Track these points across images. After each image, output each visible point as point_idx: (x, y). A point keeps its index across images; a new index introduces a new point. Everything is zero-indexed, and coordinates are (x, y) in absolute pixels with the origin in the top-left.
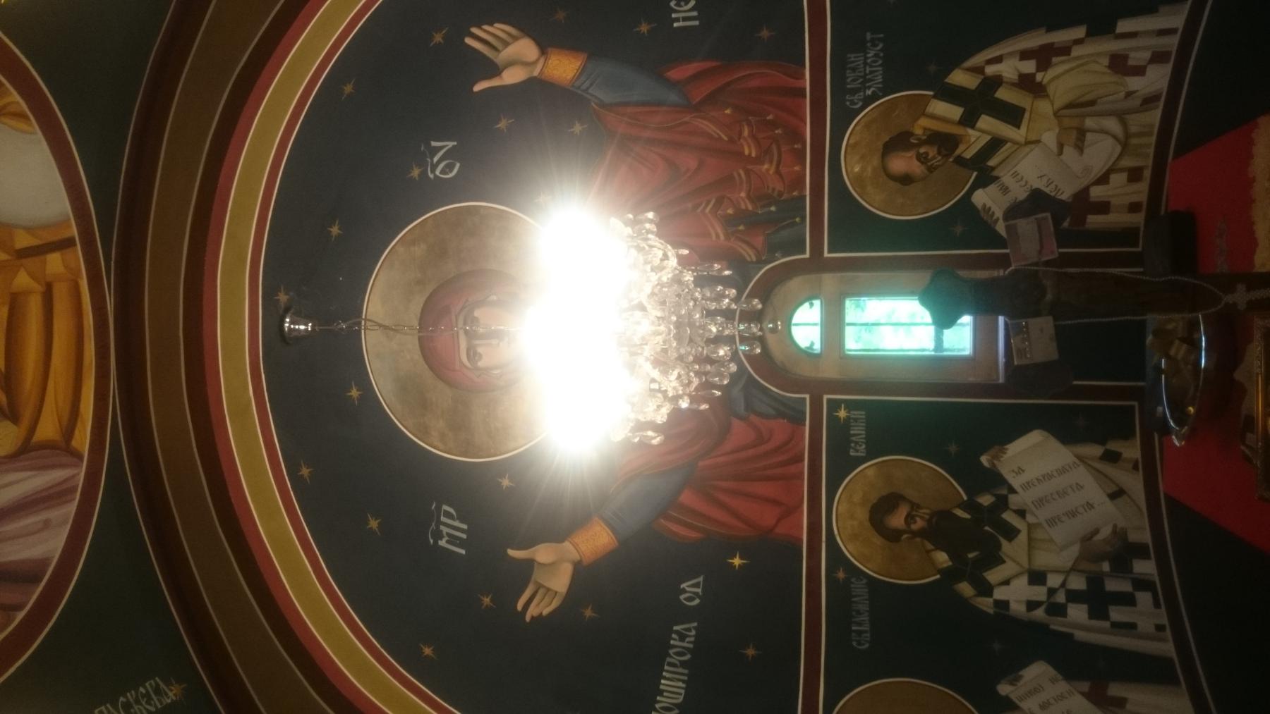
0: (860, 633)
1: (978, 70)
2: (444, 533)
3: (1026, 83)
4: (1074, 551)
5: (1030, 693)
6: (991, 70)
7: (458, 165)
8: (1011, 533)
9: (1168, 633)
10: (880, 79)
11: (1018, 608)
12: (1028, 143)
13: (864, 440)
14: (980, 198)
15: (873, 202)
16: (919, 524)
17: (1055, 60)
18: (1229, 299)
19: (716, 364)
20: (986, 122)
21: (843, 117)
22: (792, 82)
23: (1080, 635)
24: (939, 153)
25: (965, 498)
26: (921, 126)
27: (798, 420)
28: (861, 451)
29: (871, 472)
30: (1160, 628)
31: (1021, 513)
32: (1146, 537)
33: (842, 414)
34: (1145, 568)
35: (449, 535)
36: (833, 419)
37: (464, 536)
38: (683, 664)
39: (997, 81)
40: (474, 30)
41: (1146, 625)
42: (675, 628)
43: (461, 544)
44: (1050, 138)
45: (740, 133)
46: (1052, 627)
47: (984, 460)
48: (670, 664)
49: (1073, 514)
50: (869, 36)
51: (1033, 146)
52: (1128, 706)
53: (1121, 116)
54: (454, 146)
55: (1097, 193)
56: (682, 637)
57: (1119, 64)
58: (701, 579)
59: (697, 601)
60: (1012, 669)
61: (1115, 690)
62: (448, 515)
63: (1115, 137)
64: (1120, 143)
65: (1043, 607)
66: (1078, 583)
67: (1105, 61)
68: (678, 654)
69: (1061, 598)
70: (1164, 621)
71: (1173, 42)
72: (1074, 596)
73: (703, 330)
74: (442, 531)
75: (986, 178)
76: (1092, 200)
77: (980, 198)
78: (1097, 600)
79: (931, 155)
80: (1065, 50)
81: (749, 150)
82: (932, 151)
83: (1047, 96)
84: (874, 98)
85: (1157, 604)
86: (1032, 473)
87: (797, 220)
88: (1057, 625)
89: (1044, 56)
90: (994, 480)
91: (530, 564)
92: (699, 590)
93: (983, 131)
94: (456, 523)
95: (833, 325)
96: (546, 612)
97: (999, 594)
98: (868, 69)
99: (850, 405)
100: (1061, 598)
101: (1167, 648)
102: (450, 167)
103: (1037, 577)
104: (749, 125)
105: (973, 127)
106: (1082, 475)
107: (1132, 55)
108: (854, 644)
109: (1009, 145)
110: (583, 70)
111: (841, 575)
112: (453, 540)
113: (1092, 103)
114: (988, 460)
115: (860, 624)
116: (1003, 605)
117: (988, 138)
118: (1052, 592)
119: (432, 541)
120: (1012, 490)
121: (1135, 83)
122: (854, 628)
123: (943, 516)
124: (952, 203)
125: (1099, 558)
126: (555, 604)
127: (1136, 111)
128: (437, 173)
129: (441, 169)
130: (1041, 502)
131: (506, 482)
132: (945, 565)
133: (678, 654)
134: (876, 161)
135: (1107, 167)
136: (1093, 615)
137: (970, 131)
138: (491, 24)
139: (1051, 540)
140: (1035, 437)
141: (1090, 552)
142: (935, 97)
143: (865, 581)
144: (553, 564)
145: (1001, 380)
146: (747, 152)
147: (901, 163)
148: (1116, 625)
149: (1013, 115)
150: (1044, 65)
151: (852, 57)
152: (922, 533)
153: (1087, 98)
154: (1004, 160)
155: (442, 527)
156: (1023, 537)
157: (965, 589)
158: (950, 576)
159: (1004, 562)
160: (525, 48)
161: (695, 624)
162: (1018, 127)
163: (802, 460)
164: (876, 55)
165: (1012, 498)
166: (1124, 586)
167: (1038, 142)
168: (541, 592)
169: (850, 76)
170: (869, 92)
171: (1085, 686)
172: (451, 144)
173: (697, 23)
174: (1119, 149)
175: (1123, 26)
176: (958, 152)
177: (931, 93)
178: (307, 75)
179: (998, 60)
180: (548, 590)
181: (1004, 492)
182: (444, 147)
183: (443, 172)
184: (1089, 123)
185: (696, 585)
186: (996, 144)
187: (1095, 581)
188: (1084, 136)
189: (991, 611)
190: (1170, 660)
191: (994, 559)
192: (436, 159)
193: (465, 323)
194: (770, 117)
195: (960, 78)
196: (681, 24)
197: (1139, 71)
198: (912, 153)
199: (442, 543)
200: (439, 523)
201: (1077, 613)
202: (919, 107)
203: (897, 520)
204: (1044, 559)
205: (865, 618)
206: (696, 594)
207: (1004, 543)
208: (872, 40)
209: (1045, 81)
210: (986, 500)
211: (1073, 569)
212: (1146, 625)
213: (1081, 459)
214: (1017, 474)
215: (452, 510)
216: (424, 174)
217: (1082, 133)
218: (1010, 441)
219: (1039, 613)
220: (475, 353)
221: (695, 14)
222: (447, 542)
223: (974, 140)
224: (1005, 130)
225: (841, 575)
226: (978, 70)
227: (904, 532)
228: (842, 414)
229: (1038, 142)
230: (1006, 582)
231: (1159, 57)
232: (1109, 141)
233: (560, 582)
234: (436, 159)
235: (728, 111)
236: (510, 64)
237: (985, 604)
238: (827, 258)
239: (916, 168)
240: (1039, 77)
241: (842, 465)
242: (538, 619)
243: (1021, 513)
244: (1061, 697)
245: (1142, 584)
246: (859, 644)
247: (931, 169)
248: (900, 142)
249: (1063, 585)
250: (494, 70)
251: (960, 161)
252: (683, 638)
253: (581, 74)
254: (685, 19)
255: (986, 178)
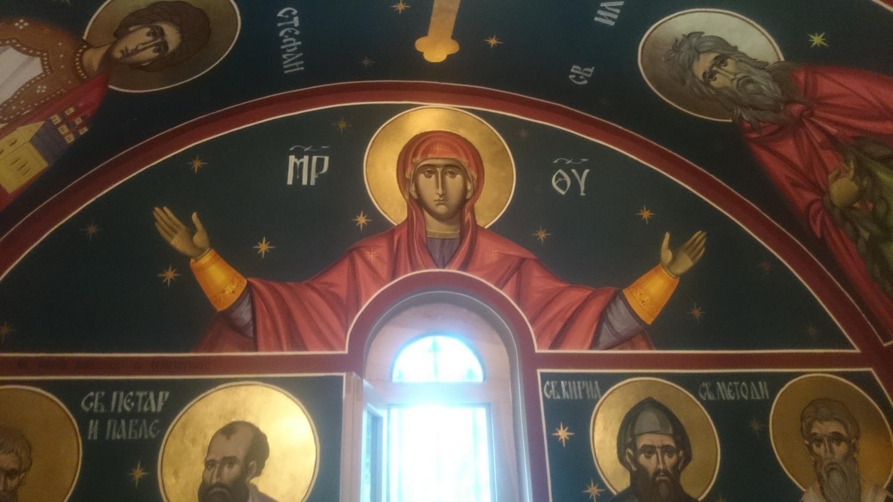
2: (301, 160)
7: (563, 193)
13: (739, 398)
19: (608, 311)
35: (302, 164)
62: (320, 163)
74: (303, 157)
102: (562, 185)
112: (298, 170)
119: (292, 149)
122: (562, 383)
161: (621, 3)
178: (567, 106)
199: (292, 159)
200: (311, 155)
215: (325, 169)
222: (295, 164)
234: (574, 171)
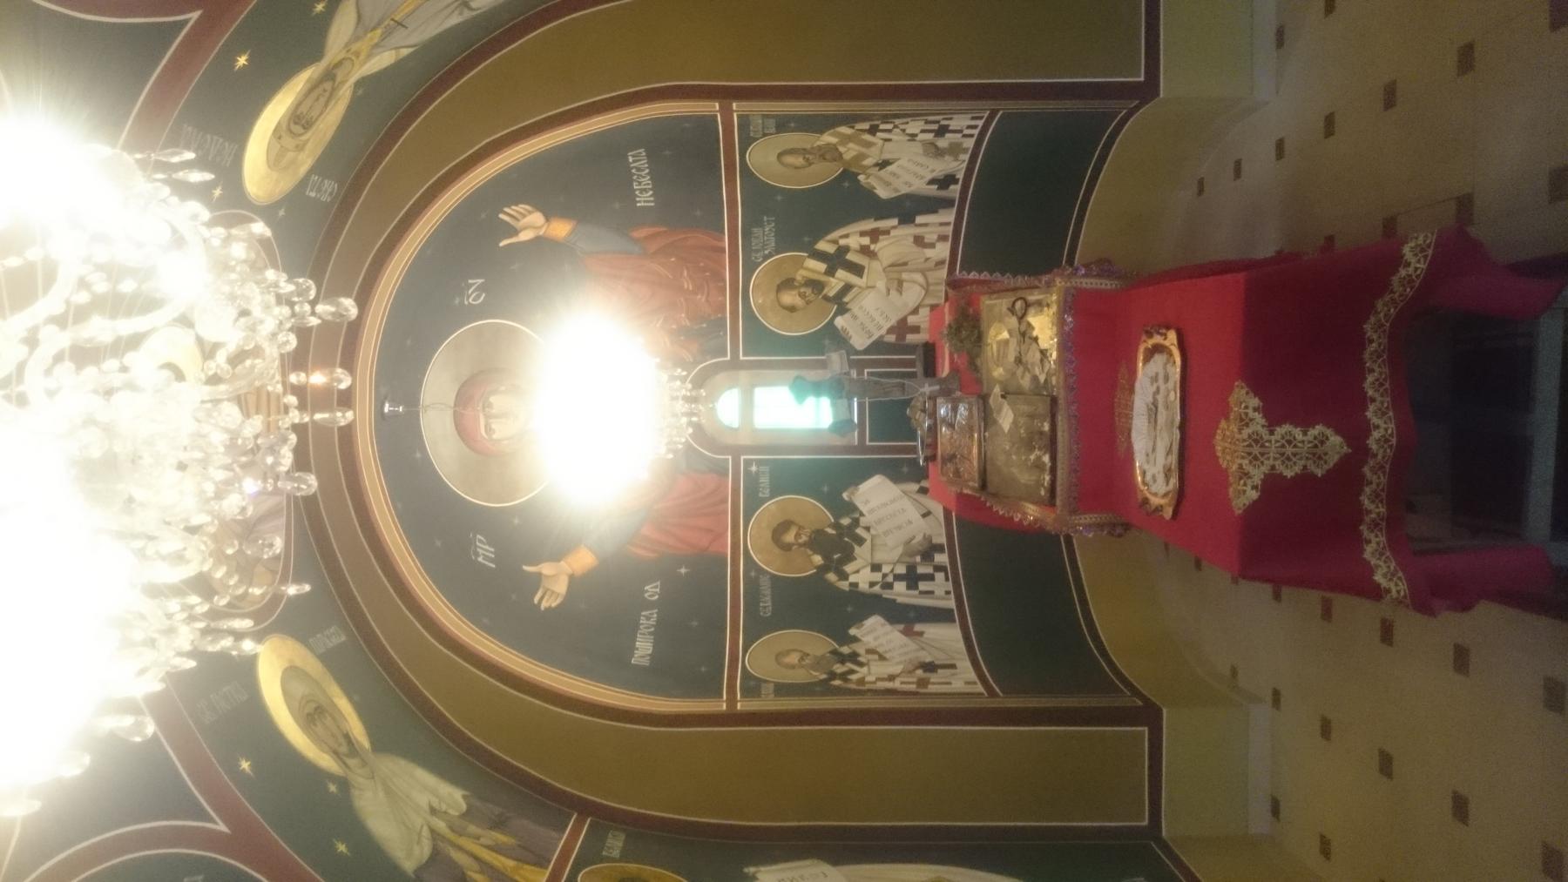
0: (765, 607)
1: (835, 242)
3: (865, 250)
4: (900, 550)
5: (869, 633)
6: (842, 242)
7: (484, 295)
8: (861, 541)
9: (952, 595)
10: (773, 245)
11: (864, 586)
12: (868, 287)
14: (840, 322)
15: (772, 323)
16: (804, 539)
17: (881, 237)
18: (922, 390)
20: (841, 273)
21: (750, 268)
22: (719, 244)
23: (900, 600)
24: (813, 292)
25: (833, 520)
26: (800, 275)
27: (723, 473)
28: (767, 493)
29: (773, 507)
30: (948, 593)
31: (868, 529)
32: (943, 540)
33: (754, 468)
34: (942, 558)
35: (484, 555)
36: (747, 473)
37: (493, 556)
38: (650, 633)
39: (846, 249)
40: (506, 210)
41: (940, 592)
42: (643, 613)
43: (491, 560)
44: (881, 285)
45: (682, 274)
46: (884, 596)
47: (845, 496)
48: (640, 634)
49: (899, 527)
50: (765, 218)
51: (870, 289)
52: (925, 636)
53: (923, 272)
54: (483, 283)
55: (912, 320)
56: (648, 618)
57: (919, 241)
58: (659, 583)
59: (657, 597)
60: (859, 619)
61: (918, 627)
62: (480, 541)
63: (921, 286)
64: (924, 288)
65: (879, 585)
66: (901, 570)
67: (912, 239)
68: (645, 628)
69: (890, 579)
70: (951, 589)
71: (949, 230)
72: (898, 577)
73: (237, 439)
75: (843, 310)
76: (909, 324)
77: (840, 322)
78: (912, 579)
79: (807, 294)
80: (887, 232)
81: (689, 286)
82: (808, 291)
83: (878, 259)
84: (770, 255)
85: (947, 579)
86: (873, 504)
87: (721, 333)
88: (887, 594)
89: (875, 235)
90: (851, 508)
91: (540, 575)
92: (658, 590)
93: (840, 280)
94: (487, 547)
95: (748, 404)
96: (554, 605)
97: (852, 579)
98: (766, 238)
99: (759, 463)
100: (890, 579)
101: (951, 603)
102: (478, 297)
103: (876, 568)
104: (687, 268)
105: (833, 276)
106: (906, 504)
107: (927, 236)
108: (762, 614)
109: (855, 289)
110: (572, 232)
111: (753, 574)
112: (486, 558)
113: (905, 264)
114: (848, 496)
115: (765, 602)
116: (855, 585)
117: (842, 284)
118: (885, 576)
120: (862, 514)
121: (929, 253)
123: (819, 533)
124: (823, 324)
125: (913, 555)
126: (559, 601)
127: (930, 270)
128: (470, 300)
129: (473, 296)
130: (879, 521)
131: (516, 521)
132: (820, 563)
133: (645, 628)
134: (772, 296)
135: (917, 304)
136: (909, 587)
137: (831, 279)
138: (516, 205)
139: (886, 545)
140: (877, 480)
141: (909, 552)
142: (808, 257)
143: (768, 577)
144: (554, 576)
145: (856, 443)
146: (686, 286)
147: (789, 298)
148: (921, 593)
149: (857, 270)
150: (875, 240)
151: (755, 230)
152: (804, 545)
153: (901, 262)
154: (855, 297)
155: (478, 550)
156: (868, 543)
157: (831, 577)
158: (823, 569)
159: (856, 559)
160: (537, 218)
162: (861, 277)
163: (727, 502)
164: (770, 230)
165: (862, 520)
166: (928, 570)
167: (873, 287)
168: (548, 593)
169: (754, 242)
170: (766, 252)
171: (901, 627)
172: (480, 281)
173: (652, 204)
174: (923, 292)
175: (920, 219)
176: (825, 292)
177: (806, 254)
179: (846, 236)
180: (553, 592)
181: (857, 515)
182: (475, 283)
183: (474, 300)
184: (905, 276)
185: (656, 587)
186: (847, 288)
187: (911, 568)
188: (902, 285)
189: (847, 589)
190: (952, 610)
191: (849, 557)
192: (470, 292)
193: (484, 408)
194: (702, 264)
195: (823, 246)
196: (643, 204)
197: (932, 246)
198: (795, 292)
199: (480, 559)
201: (900, 587)
202: (799, 263)
203: (789, 537)
204: (880, 557)
205: (768, 598)
206: (656, 592)
207: (856, 547)
208: (768, 221)
209: (876, 250)
210: (845, 521)
211: (898, 561)
212: (940, 592)
213: (904, 492)
214: (304, 128)
215: (482, 539)
216: (462, 302)
217: (900, 283)
218: (861, 482)
219: (877, 589)
220: (490, 429)
221: (652, 199)
223: (834, 285)
224: (853, 279)
225: (753, 574)
226: (835, 242)
227: (793, 544)
228: (754, 468)
229: (873, 287)
230: (857, 572)
231: (943, 238)
232: (918, 288)
233: (561, 587)
234: (470, 292)
235: (673, 259)
236: (525, 228)
237: (844, 585)
238: (743, 361)
239: (798, 301)
240: (872, 247)
241: (753, 503)
242: (548, 609)
243: (868, 529)
244: (887, 634)
245: (939, 568)
246: (765, 613)
247: (808, 303)
248: (787, 284)
249: (892, 571)
250: (514, 232)
251: (826, 298)
252: (648, 620)
253: (571, 234)
254: (645, 202)
255: (843, 310)
